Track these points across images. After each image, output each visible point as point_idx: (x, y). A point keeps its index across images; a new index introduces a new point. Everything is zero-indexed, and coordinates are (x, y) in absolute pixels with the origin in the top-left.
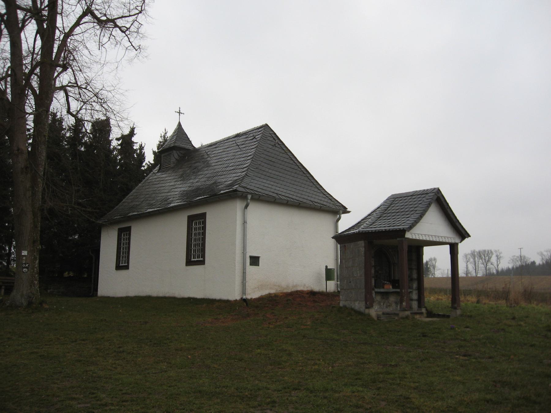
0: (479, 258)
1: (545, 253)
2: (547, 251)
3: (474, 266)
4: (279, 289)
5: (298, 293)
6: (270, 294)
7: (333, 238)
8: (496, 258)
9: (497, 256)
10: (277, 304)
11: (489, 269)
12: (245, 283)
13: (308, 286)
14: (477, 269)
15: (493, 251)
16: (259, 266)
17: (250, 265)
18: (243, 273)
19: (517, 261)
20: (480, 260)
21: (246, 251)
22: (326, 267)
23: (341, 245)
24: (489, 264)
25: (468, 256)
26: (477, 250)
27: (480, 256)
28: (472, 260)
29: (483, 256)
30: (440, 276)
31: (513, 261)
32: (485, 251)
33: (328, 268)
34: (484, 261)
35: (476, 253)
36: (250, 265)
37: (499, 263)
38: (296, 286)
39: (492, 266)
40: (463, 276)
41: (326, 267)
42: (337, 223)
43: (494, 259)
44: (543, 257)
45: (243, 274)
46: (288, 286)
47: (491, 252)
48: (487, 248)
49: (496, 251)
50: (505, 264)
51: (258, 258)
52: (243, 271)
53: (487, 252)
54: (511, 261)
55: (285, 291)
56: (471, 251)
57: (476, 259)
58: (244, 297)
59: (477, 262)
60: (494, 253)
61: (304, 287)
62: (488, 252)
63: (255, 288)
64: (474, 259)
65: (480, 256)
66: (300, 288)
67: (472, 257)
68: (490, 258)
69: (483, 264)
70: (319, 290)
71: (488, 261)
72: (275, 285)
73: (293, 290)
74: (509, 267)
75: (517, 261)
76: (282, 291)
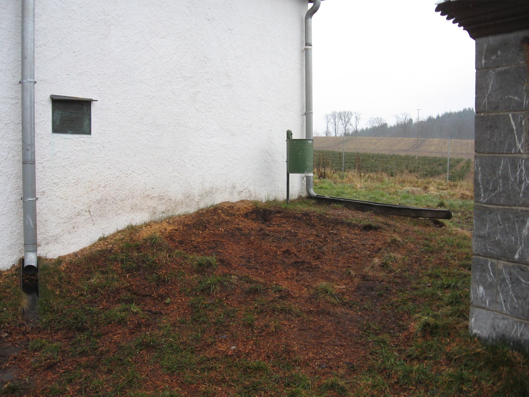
0: (339, 119)
1: (400, 116)
2: (402, 114)
3: (334, 127)
4: (161, 208)
5: (219, 217)
6: (132, 230)
7: (437, 10)
8: (355, 119)
9: (356, 117)
10: (162, 291)
11: (348, 130)
12: (34, 202)
13: (241, 189)
14: (337, 130)
15: (353, 112)
16: (89, 133)
17: (56, 129)
18: (24, 163)
19: (374, 122)
20: (340, 121)
21: (33, 77)
22: (289, 134)
23: (492, 40)
24: (348, 125)
25: (329, 117)
26: (338, 111)
27: (340, 117)
28: (332, 120)
29: (343, 117)
30: (315, 136)
31: (370, 122)
32: (345, 112)
33: (294, 137)
34: (344, 122)
35: (336, 114)
36: (56, 129)
37: (357, 124)
38: (209, 193)
39: (350, 127)
40: (322, 136)
41: (289, 134)
42: (309, 20)
43: (353, 120)
44: (399, 119)
45: (23, 170)
46: (188, 196)
47: (351, 113)
48: (347, 109)
49: (355, 113)
50: (363, 125)
51: (85, 104)
52: (24, 155)
53: (347, 114)
54: (369, 122)
55: (181, 211)
56: (332, 112)
57: (337, 119)
58: (31, 260)
59: (337, 123)
60: (353, 114)
61: (232, 193)
62: (348, 113)
63: (79, 214)
64: (335, 119)
65: (340, 117)
66: (218, 199)
67: (332, 117)
68: (349, 119)
69: (343, 124)
70: (268, 196)
71: (348, 122)
72: (148, 196)
73: (202, 205)
74: (363, 129)
75: (374, 122)
76: (170, 214)
